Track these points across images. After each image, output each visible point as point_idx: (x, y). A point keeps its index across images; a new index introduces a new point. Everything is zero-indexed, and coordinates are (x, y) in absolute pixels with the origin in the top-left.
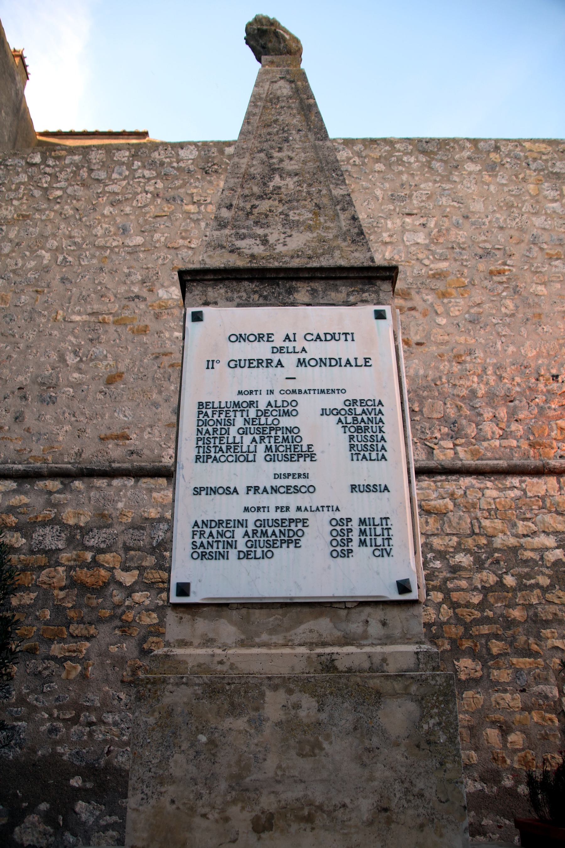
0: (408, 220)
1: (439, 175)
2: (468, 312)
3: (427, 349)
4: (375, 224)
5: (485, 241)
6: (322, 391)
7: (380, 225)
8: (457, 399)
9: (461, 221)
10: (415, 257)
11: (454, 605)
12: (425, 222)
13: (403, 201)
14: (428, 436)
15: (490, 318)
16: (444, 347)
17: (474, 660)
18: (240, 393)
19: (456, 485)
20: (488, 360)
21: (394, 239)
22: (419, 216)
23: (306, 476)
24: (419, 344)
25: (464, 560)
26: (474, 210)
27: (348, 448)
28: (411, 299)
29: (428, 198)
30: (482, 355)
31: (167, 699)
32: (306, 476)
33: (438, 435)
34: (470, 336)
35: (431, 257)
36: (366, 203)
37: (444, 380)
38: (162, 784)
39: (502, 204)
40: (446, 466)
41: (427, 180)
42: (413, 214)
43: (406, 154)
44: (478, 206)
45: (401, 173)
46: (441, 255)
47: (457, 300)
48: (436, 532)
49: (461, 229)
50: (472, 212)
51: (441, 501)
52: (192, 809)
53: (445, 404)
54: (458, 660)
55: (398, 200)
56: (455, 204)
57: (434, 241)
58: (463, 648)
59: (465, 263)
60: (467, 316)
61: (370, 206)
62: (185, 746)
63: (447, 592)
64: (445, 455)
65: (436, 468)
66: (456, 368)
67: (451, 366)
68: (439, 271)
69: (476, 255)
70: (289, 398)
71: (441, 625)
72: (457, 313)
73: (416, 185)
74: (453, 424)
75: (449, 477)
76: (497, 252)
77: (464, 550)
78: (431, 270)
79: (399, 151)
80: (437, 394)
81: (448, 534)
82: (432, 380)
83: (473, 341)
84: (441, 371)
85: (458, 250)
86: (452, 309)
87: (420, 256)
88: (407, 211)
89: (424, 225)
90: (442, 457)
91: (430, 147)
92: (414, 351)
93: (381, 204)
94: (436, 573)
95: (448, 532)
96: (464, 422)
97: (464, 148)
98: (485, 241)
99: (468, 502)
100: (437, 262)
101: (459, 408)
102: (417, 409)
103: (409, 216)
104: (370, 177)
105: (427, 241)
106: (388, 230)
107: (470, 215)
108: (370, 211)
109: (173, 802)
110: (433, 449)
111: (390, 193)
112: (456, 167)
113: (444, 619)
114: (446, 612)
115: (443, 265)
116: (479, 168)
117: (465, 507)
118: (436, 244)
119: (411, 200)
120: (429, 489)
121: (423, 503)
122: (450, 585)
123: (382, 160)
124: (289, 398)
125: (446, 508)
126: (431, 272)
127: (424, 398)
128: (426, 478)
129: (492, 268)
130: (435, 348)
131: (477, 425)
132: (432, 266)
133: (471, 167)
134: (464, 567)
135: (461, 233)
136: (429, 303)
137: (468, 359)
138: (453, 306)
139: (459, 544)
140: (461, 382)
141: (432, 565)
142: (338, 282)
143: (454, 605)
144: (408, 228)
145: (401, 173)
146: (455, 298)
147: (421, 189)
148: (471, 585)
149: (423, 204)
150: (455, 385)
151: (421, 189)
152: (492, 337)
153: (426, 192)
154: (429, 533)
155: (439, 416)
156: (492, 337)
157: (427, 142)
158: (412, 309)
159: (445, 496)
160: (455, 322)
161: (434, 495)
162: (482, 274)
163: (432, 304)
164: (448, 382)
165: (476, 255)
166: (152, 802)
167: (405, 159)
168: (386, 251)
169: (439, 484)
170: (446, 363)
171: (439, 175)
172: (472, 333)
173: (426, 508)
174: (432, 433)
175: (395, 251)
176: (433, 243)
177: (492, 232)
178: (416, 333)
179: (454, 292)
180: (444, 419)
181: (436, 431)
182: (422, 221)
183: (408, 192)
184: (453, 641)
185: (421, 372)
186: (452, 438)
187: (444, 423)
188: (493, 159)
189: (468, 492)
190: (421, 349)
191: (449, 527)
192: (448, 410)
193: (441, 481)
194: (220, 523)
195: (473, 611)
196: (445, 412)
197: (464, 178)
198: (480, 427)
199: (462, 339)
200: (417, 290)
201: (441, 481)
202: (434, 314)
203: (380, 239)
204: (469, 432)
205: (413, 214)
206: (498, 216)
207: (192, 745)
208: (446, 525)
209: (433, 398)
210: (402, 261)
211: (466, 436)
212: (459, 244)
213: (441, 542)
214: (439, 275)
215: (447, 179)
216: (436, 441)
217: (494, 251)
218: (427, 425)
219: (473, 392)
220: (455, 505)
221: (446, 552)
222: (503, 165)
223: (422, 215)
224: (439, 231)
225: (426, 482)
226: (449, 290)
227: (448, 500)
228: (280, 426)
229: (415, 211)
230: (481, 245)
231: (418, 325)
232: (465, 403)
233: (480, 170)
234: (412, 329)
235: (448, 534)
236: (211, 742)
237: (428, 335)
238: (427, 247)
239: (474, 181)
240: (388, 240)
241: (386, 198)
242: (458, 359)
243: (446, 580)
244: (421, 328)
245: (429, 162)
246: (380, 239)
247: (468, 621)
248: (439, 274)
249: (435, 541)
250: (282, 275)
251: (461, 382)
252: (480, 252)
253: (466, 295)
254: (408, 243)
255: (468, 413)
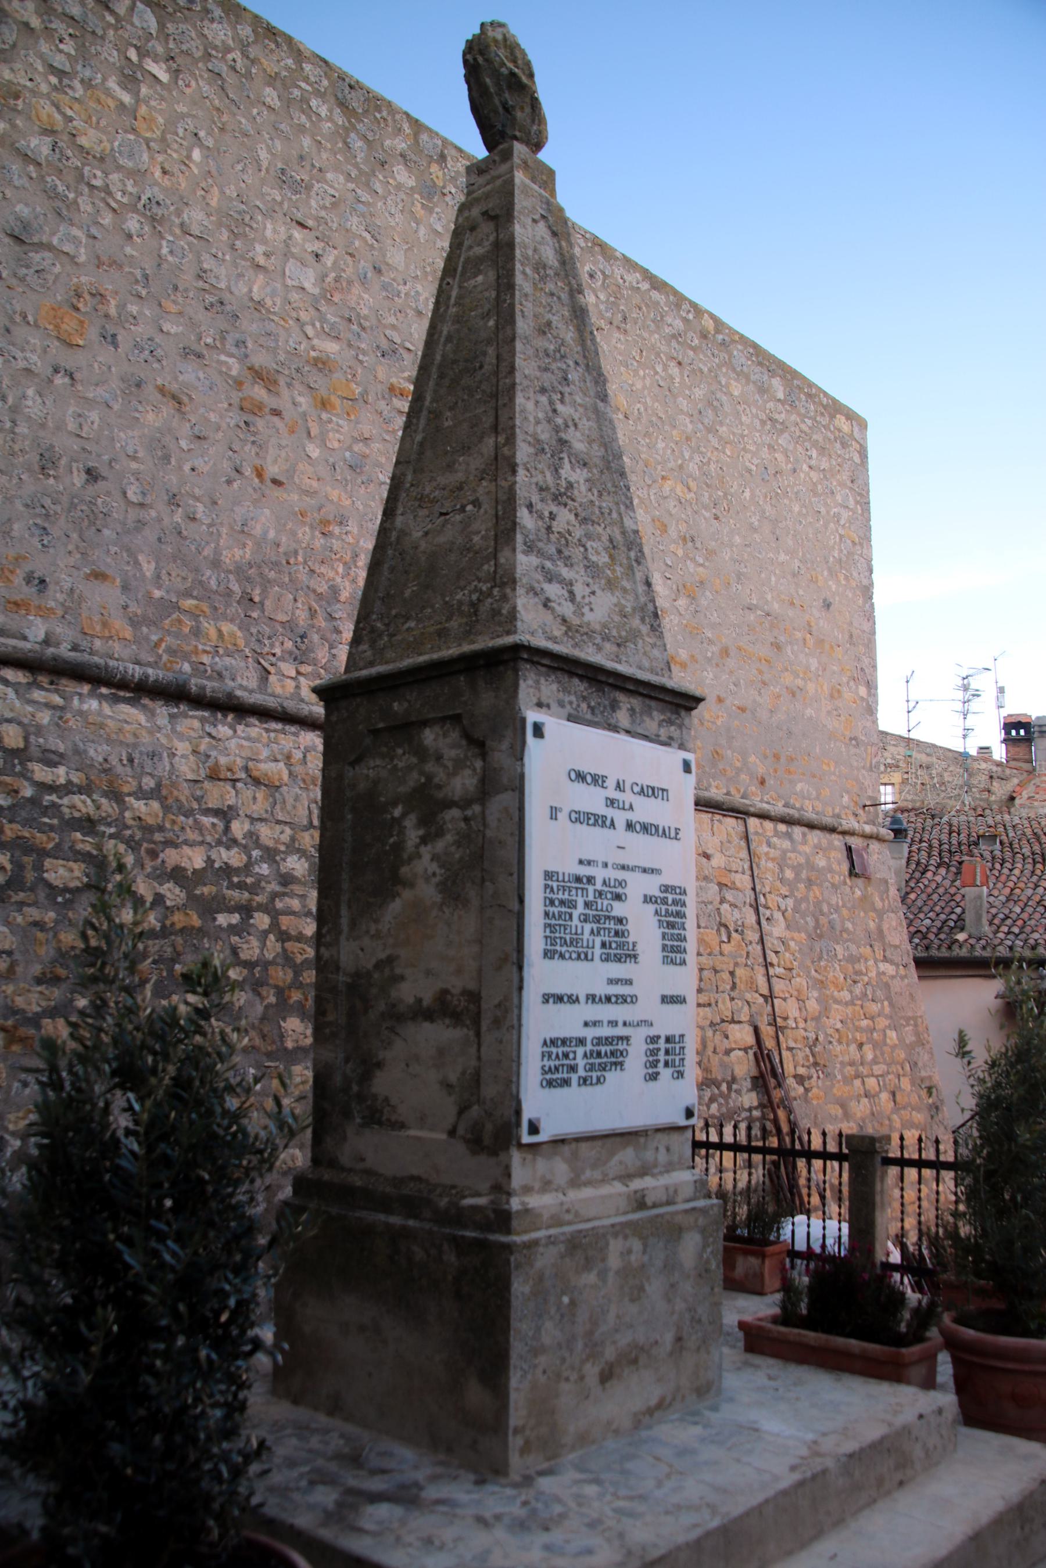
0: (298, 234)
1: (356, 166)
2: (350, 449)
3: (285, 496)
4: (247, 218)
5: (393, 327)
6: (645, 871)
7: (255, 226)
8: (312, 596)
9: (369, 275)
10: (294, 314)
11: (284, 937)
12: (320, 252)
13: (296, 193)
14: (266, 650)
15: (377, 470)
16: (308, 499)
17: (302, 1021)
18: (581, 862)
19: (295, 742)
20: (361, 543)
21: (271, 263)
22: (314, 233)
23: (629, 982)
24: (276, 482)
25: (297, 866)
26: (390, 262)
27: (660, 948)
28: (277, 394)
29: (334, 205)
30: (355, 531)
31: (539, 1264)
32: (629, 982)
33: (278, 651)
34: (346, 492)
35: (318, 325)
36: (239, 167)
37: (300, 559)
38: (536, 1356)
39: (428, 269)
40: (289, 710)
41: (337, 169)
42: (306, 227)
43: (318, 93)
44: (396, 257)
45: (301, 129)
46: (333, 326)
47: (341, 422)
48: (264, 816)
49: (367, 290)
50: (388, 264)
51: (273, 765)
52: (558, 1376)
53: (295, 600)
54: (285, 1021)
55: (290, 187)
56: (368, 237)
57: (327, 295)
58: (291, 1001)
59: (361, 357)
60: (348, 454)
61: (245, 177)
62: (553, 1311)
63: (275, 915)
64: (283, 687)
65: (275, 710)
66: (319, 542)
67: (313, 537)
68: (324, 358)
69: (378, 347)
70: (621, 875)
71: (266, 964)
72: (336, 445)
73: (320, 170)
74: (302, 637)
75: (287, 727)
76: (405, 355)
77: (298, 851)
78: (314, 349)
79: (306, 80)
80: (287, 579)
81: (278, 822)
82: (285, 554)
83: (348, 502)
84: (298, 542)
85: (355, 327)
86: (331, 434)
87: (304, 316)
88: (299, 216)
89: (317, 256)
90: (279, 691)
91: (356, 102)
92: (267, 492)
93: (263, 182)
94: (263, 884)
95: (280, 818)
96: (316, 638)
97: (400, 130)
98: (393, 327)
99: (307, 774)
100: (324, 336)
101: (313, 613)
102: (257, 599)
103: (300, 228)
104: (255, 111)
105: (316, 291)
106: (264, 241)
107: (383, 268)
108: (243, 185)
109: (544, 1372)
110: (269, 673)
111: (280, 165)
112: (383, 164)
113: (269, 956)
114: (273, 947)
115: (332, 347)
116: (411, 183)
117: (304, 781)
118: (329, 301)
119: (309, 197)
120: (259, 742)
121: (250, 764)
122: (279, 905)
123: (278, 84)
124: (621, 875)
125: (280, 779)
126: (313, 354)
127: (269, 581)
128: (257, 723)
129: (394, 380)
130: (296, 497)
131: (331, 647)
132: (315, 342)
133: (402, 175)
134: (297, 878)
135: (366, 296)
136: (301, 410)
137: (337, 530)
138: (333, 429)
139: (293, 839)
140: (323, 570)
141: (257, 869)
142: (653, 704)
143: (284, 937)
144: (294, 250)
145: (301, 129)
146: (337, 415)
147: (326, 182)
148: (304, 906)
149: (323, 213)
150: (313, 571)
151: (326, 182)
152: (373, 504)
153: (333, 192)
154: (255, 816)
155: (285, 619)
156: (373, 504)
157: (351, 87)
158: (276, 413)
159: (279, 757)
160: (331, 460)
161: (265, 753)
162: (379, 386)
163: (304, 414)
164: (305, 562)
165: (378, 347)
166: (529, 1377)
167: (314, 103)
168: (254, 282)
169: (272, 735)
170: (307, 529)
171: (356, 166)
172: (349, 488)
173: (255, 773)
174: (272, 646)
175: (268, 290)
176: (325, 298)
177: (407, 315)
178: (275, 461)
179: (337, 402)
180: (290, 625)
181: (277, 644)
182: (317, 246)
183: (306, 178)
184: (280, 992)
185: (272, 534)
186: (295, 659)
187: (289, 634)
188: (434, 176)
189: (309, 757)
190: (277, 492)
191: (282, 809)
192: (298, 612)
193: (275, 731)
194: (564, 1041)
195: (305, 947)
196: (293, 614)
197: (390, 193)
198: (334, 651)
199: (334, 494)
200: (288, 380)
201: (275, 731)
202: (305, 435)
203: (251, 254)
204: (320, 656)
205: (306, 227)
206: (419, 288)
207: (558, 1309)
208: (278, 807)
209: (281, 585)
210: (274, 313)
211: (314, 662)
212: (358, 315)
213: (269, 832)
214: (321, 364)
215: (365, 180)
216: (273, 660)
217: (401, 351)
218: (267, 630)
219: (335, 590)
220: (291, 774)
221: (276, 851)
222: (444, 195)
223: (318, 234)
224: (337, 280)
225: (257, 729)
226: (333, 398)
227: (281, 765)
228: (613, 914)
229: (310, 223)
230: (388, 332)
231: (280, 447)
232: (321, 607)
233: (412, 188)
234: (271, 451)
235: (278, 822)
236: (573, 1303)
237: (291, 471)
238: (315, 299)
239: (400, 206)
240: (261, 260)
241: (272, 172)
242: (323, 527)
243: (274, 895)
244: (283, 454)
245: (347, 130)
246: (251, 254)
247: (299, 961)
248: (324, 363)
249: (262, 830)
250: (611, 681)
251: (323, 570)
252: (385, 344)
253: (353, 417)
254: (289, 282)
255: (323, 624)
